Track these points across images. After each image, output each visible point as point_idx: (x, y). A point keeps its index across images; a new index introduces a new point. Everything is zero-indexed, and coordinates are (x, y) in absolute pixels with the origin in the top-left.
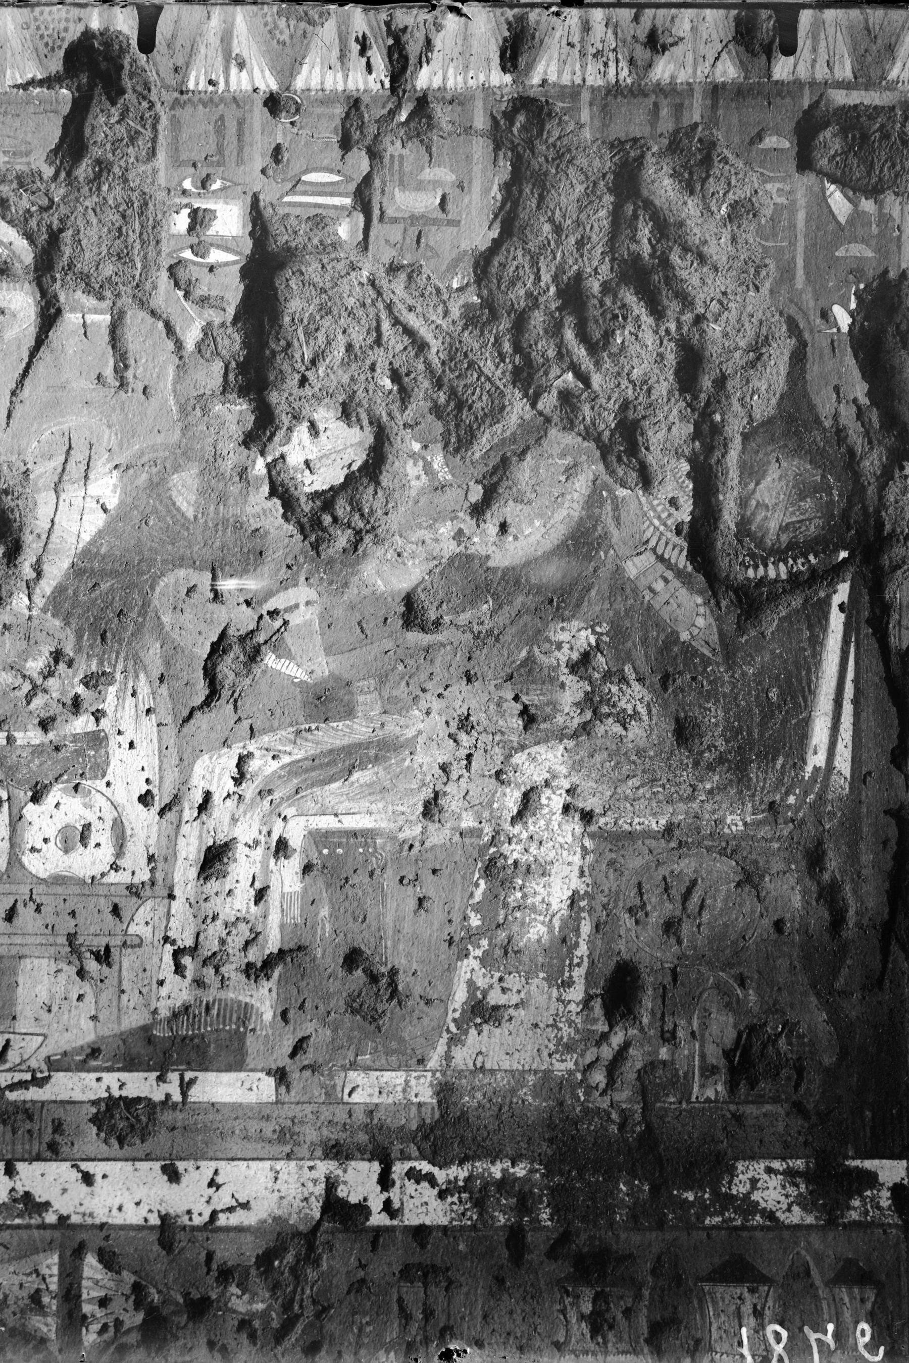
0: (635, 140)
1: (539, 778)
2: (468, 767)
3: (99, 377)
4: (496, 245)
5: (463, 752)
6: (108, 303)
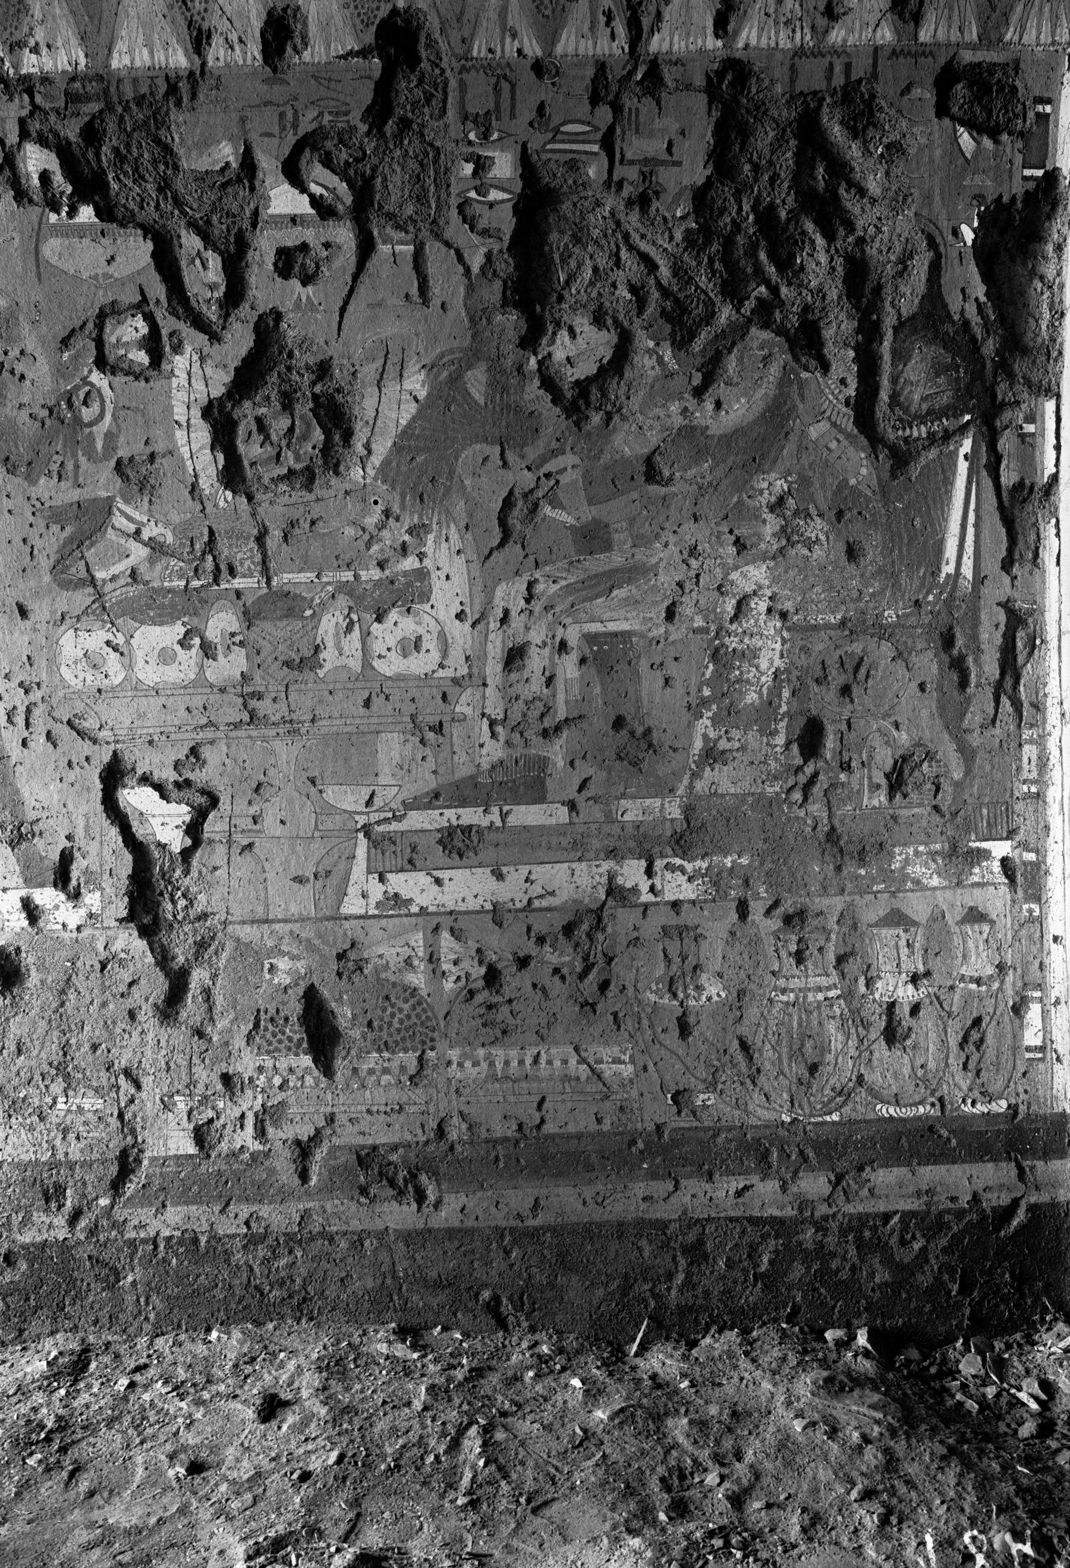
0: (815, 93)
1: (749, 588)
2: (697, 584)
3: (407, 296)
4: (709, 183)
5: (693, 573)
6: (411, 236)
